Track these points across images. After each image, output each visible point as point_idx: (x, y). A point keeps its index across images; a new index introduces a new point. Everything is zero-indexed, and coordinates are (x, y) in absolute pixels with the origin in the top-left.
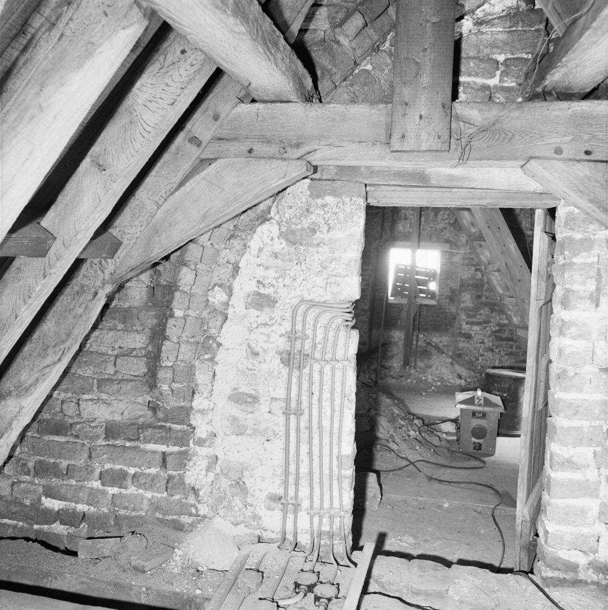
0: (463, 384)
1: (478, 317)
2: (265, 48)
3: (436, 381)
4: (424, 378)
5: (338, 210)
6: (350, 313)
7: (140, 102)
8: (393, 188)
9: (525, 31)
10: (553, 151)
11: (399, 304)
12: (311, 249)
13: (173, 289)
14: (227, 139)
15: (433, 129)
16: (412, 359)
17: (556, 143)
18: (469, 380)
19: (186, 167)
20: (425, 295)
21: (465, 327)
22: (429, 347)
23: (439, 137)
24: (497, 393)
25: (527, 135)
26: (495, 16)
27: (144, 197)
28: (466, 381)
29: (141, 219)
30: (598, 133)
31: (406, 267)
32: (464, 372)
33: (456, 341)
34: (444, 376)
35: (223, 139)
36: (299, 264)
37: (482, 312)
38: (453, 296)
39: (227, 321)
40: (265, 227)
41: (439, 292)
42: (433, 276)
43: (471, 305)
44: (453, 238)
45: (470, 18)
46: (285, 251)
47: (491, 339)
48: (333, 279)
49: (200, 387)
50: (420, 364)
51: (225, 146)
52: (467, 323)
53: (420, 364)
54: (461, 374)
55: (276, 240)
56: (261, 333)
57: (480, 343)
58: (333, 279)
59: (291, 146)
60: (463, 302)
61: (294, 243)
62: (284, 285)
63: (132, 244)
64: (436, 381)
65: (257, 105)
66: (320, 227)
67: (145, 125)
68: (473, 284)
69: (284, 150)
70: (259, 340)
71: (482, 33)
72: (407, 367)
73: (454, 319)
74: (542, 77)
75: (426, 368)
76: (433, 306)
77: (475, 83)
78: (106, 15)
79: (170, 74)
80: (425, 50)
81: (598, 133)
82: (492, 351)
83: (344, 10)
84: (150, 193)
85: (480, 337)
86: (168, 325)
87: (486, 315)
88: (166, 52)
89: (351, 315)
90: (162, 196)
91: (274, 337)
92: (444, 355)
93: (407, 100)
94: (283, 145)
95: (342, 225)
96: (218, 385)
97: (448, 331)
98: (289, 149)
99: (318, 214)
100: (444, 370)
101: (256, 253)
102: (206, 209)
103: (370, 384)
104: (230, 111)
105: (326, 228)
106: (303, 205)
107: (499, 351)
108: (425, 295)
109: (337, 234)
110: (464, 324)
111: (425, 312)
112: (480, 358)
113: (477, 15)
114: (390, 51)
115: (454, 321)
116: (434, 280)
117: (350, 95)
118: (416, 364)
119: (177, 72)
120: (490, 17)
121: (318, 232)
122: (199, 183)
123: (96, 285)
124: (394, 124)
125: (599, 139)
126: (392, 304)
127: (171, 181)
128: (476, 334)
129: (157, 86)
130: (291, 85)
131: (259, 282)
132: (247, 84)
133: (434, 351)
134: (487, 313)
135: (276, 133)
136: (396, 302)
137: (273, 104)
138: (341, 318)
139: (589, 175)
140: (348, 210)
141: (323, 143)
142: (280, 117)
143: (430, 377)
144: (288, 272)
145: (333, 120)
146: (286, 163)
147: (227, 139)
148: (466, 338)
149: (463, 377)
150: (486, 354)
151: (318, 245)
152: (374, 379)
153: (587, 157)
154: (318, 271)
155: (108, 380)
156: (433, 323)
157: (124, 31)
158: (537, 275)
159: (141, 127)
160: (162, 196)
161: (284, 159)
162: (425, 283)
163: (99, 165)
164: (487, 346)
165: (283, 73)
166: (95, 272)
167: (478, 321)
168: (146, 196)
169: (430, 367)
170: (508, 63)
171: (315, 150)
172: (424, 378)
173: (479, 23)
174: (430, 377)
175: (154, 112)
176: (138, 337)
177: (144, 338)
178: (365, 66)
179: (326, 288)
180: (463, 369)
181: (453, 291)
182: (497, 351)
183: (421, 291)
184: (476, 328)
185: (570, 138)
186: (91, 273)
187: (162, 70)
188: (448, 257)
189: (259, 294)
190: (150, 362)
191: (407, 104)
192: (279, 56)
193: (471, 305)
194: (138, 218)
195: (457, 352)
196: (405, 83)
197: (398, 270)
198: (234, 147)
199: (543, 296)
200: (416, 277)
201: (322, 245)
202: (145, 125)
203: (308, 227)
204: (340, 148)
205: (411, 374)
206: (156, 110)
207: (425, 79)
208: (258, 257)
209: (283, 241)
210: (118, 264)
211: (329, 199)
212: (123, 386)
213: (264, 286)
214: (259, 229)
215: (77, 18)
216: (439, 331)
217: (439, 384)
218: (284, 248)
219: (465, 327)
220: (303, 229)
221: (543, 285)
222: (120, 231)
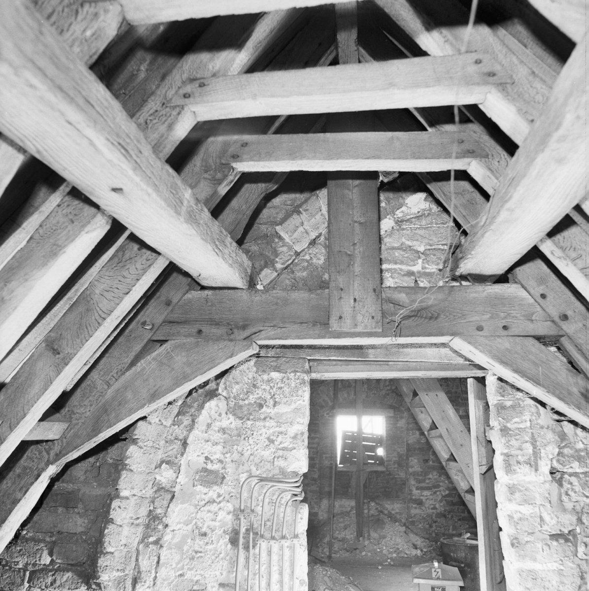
0: (419, 555)
1: (427, 481)
2: (214, 247)
3: (391, 553)
4: (378, 550)
5: (283, 385)
6: (298, 487)
7: (97, 292)
8: (334, 363)
9: (439, 227)
10: (475, 328)
11: (348, 472)
12: (258, 423)
13: (120, 467)
14: (178, 323)
15: (367, 311)
16: (365, 530)
17: (478, 321)
18: (425, 550)
19: (138, 348)
20: (373, 462)
21: (416, 492)
22: (382, 516)
23: (373, 317)
24: (454, 563)
25: (450, 314)
26: (412, 216)
27: (96, 377)
28: (422, 551)
29: (90, 398)
30: (512, 312)
31: (353, 433)
32: (419, 542)
33: (408, 508)
34: (399, 547)
35: (174, 322)
36: (247, 439)
37: (430, 476)
38: (402, 462)
39: (174, 500)
40: (211, 405)
41: (387, 457)
42: (379, 441)
43: (419, 469)
44: (396, 403)
45: (391, 218)
46: (233, 426)
47: (442, 504)
48: (280, 453)
49: (143, 575)
50: (374, 535)
51: (175, 328)
52: (417, 489)
53: (374, 535)
54: (416, 543)
55: (224, 415)
56: (209, 511)
57: (432, 509)
58: (280, 453)
59: (238, 328)
60: (412, 467)
61: (241, 418)
62: (232, 461)
63: (80, 424)
64: (391, 553)
65: (206, 292)
66: (266, 402)
67: (100, 312)
68: (419, 448)
69: (231, 332)
70: (206, 519)
71: (403, 229)
72: (361, 539)
73: (404, 484)
74: (456, 266)
75: (380, 539)
76: (383, 472)
77: (401, 270)
78: (73, 222)
79: (127, 267)
80: (354, 244)
81: (512, 312)
82: (445, 516)
83: (284, 211)
84: (102, 373)
85: (431, 502)
86: (113, 507)
87: (435, 479)
88: (124, 249)
89: (300, 490)
90: (113, 376)
91: (222, 515)
92: (397, 524)
93: (341, 286)
94: (230, 327)
95: (287, 399)
96: (163, 572)
97: (399, 497)
98: (235, 331)
99: (264, 389)
100: (399, 540)
101: (204, 428)
102: (157, 387)
103: (323, 560)
104: (182, 298)
105: (272, 402)
106: (250, 381)
107: (452, 517)
108: (373, 462)
109: (282, 409)
110: (414, 489)
111: (375, 479)
112: (434, 525)
113: (397, 215)
114: (325, 244)
115: (403, 486)
116: (381, 446)
117: (291, 281)
118: (369, 535)
119: (134, 266)
120: (408, 217)
121: (264, 407)
122: (150, 363)
123: (40, 467)
124: (331, 307)
125: (513, 317)
126: (342, 471)
127: (123, 362)
128: (427, 500)
129: (115, 277)
130: (237, 274)
131: (207, 458)
132: (198, 275)
133: (387, 520)
134: (435, 477)
135: (224, 316)
136: (345, 470)
137: (221, 291)
138: (290, 490)
139: (509, 348)
140: (293, 385)
141: (267, 324)
142: (228, 302)
143: (384, 548)
144: (235, 447)
145: (277, 304)
146: (233, 343)
147: (178, 323)
148: (418, 504)
149: (418, 547)
150: (439, 520)
151: (265, 419)
152: (328, 554)
153: (505, 333)
154: (265, 445)
155: (42, 570)
156: (383, 489)
157: (88, 235)
158: (476, 441)
159: (96, 314)
160: (113, 376)
161: (231, 340)
162: (372, 449)
163: (54, 350)
164: (438, 511)
165: (231, 266)
166: (40, 453)
167: (427, 485)
168: (97, 376)
169: (384, 537)
170: (428, 252)
171: (261, 331)
172: (378, 550)
173: (399, 222)
174: (384, 548)
175: (110, 300)
176: (80, 521)
177: (86, 521)
178: (303, 256)
179: (273, 462)
180: (418, 538)
181: (400, 456)
182: (450, 516)
183: (371, 457)
184: (426, 493)
185: (488, 316)
186: (35, 454)
187: (120, 264)
188: (392, 423)
189: (205, 470)
190: (90, 548)
191: (342, 289)
192: (226, 251)
193: (419, 469)
194: (88, 398)
195: (410, 520)
196: (339, 272)
197: (346, 437)
198: (184, 329)
199: (484, 462)
200: (363, 443)
201: (268, 419)
202: (100, 312)
203: (255, 402)
204: (283, 329)
205: (365, 546)
206: (112, 298)
207: (357, 268)
208: (206, 432)
209: (230, 416)
210: (64, 444)
211: (275, 375)
212: (58, 578)
213: (212, 462)
214: (207, 405)
215: (46, 225)
216: (390, 498)
217: (395, 555)
218: (231, 423)
219: (416, 492)
220: (250, 404)
221: (483, 450)
222: (68, 411)
